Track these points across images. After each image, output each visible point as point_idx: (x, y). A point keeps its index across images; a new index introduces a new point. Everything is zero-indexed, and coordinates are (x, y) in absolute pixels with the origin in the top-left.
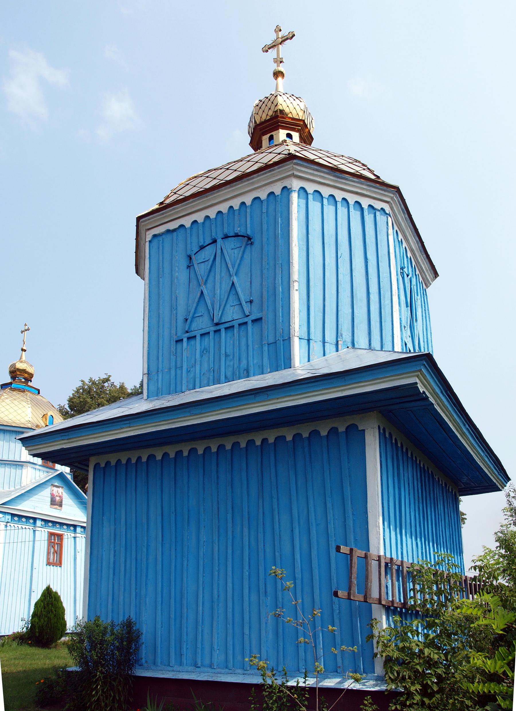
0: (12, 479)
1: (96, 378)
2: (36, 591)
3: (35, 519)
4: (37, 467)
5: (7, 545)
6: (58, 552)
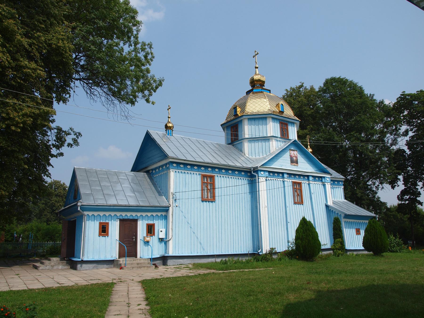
0: (264, 149)
1: (294, 86)
2: (290, 222)
3: (283, 173)
4: (278, 139)
5: (268, 191)
6: (300, 195)
